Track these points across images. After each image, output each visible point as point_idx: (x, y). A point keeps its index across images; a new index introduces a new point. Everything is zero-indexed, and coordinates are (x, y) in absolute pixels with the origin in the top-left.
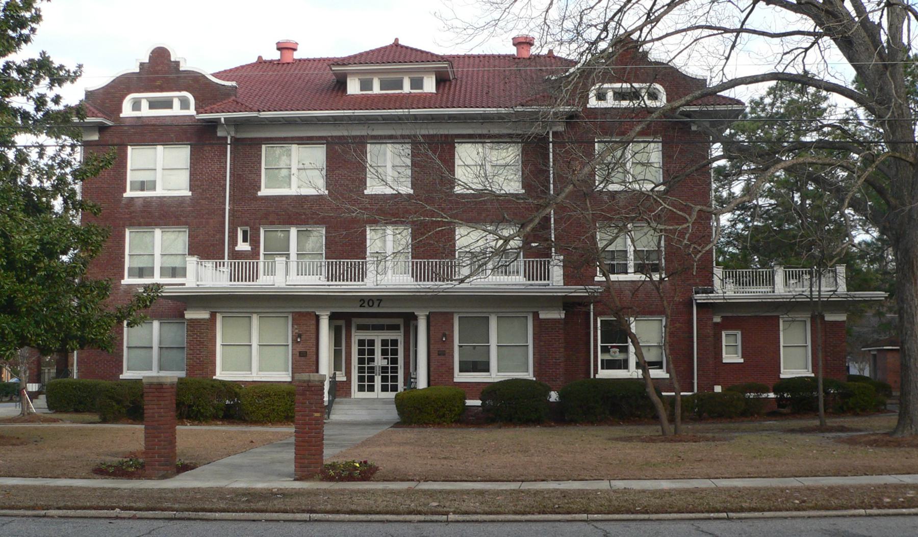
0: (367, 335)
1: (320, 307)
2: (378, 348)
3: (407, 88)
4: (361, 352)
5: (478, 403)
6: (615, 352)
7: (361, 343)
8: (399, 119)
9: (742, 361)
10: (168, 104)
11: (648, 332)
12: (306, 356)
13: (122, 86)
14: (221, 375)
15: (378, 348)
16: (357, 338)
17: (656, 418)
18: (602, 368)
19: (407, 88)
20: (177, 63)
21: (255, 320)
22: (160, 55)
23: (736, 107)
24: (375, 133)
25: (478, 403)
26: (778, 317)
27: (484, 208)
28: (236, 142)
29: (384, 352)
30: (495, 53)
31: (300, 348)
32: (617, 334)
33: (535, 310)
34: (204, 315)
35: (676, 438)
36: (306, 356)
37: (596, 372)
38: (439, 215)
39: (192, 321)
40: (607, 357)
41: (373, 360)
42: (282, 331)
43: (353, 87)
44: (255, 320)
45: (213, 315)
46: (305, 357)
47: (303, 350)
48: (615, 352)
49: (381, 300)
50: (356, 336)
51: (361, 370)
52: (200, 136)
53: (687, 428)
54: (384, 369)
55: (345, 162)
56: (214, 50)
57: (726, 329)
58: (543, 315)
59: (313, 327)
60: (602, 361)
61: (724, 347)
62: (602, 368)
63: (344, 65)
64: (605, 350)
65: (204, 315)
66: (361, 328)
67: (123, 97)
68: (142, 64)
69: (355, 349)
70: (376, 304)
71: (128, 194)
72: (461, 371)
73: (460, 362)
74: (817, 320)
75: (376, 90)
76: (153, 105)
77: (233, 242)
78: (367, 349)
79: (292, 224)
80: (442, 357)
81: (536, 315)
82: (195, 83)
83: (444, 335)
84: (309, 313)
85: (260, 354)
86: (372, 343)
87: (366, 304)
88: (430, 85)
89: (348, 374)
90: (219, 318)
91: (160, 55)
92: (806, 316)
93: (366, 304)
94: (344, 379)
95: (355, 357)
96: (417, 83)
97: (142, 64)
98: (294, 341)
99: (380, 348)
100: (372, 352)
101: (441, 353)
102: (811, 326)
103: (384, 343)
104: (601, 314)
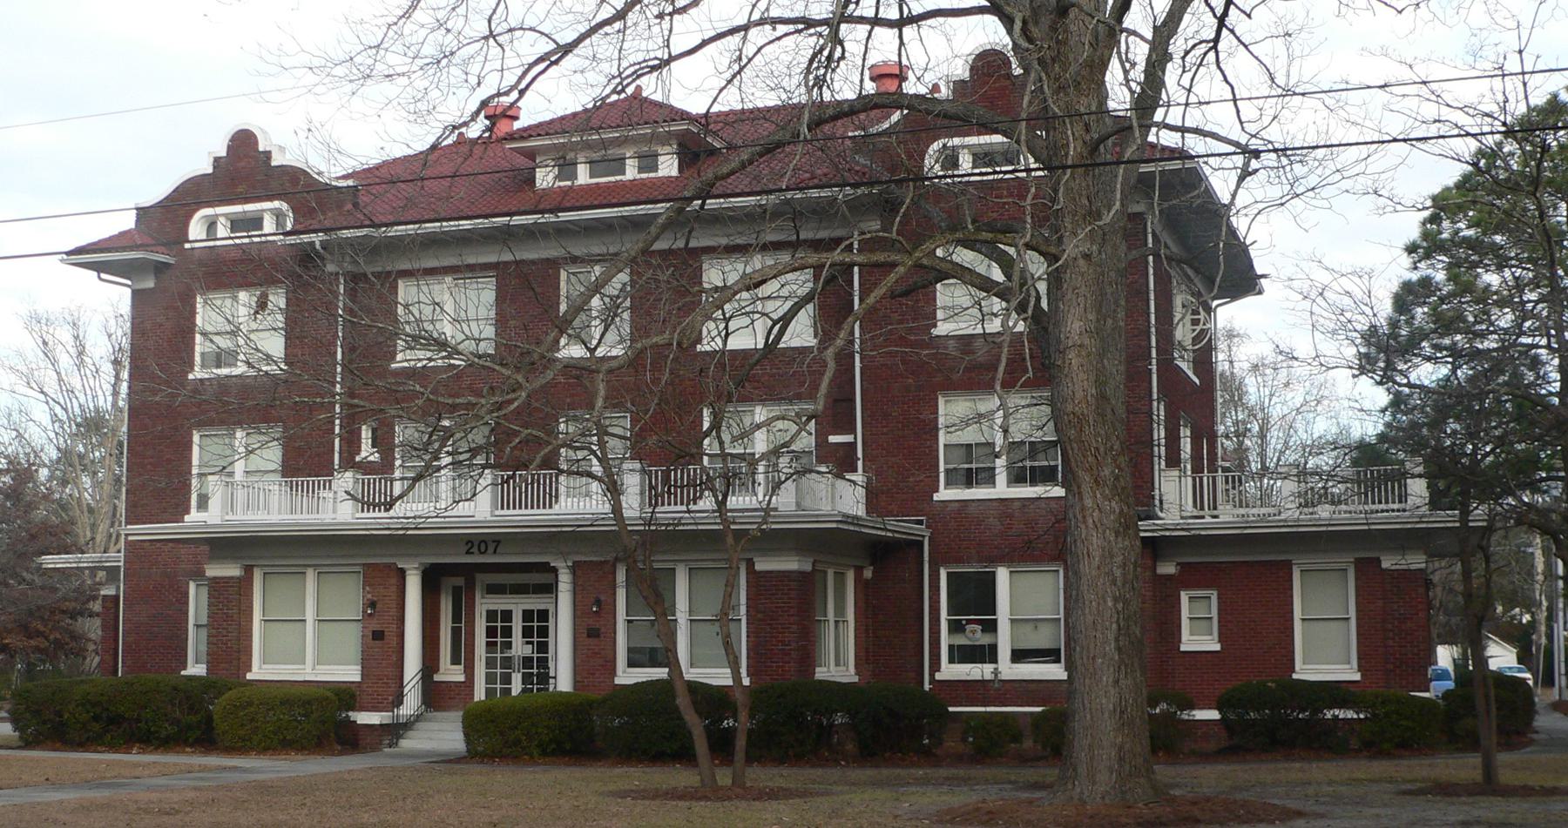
0: (499, 603)
1: (402, 555)
2: (517, 626)
3: (631, 172)
4: (491, 632)
5: (1214, 715)
6: (974, 632)
7: (491, 616)
8: (606, 226)
9: (1217, 647)
10: (236, 224)
11: (1022, 598)
12: (598, 636)
13: (189, 196)
14: (259, 671)
15: (517, 626)
16: (485, 608)
17: (685, 755)
18: (951, 661)
19: (631, 172)
20: (268, 155)
21: (311, 575)
22: (243, 141)
23: (1176, 165)
24: (471, 260)
25: (1214, 715)
26: (1288, 566)
27: (765, 374)
28: (355, 279)
29: (527, 632)
30: (568, 112)
31: (375, 625)
32: (975, 599)
33: (749, 556)
34: (232, 571)
35: (742, 792)
36: (598, 636)
37: (935, 666)
38: (510, 402)
39: (215, 580)
40: (960, 640)
41: (509, 645)
42: (349, 597)
43: (545, 178)
44: (311, 575)
45: (249, 570)
46: (381, 641)
47: (377, 628)
48: (974, 632)
49: (498, 542)
50: (484, 604)
51: (490, 663)
52: (292, 273)
53: (762, 776)
54: (527, 662)
55: (528, 300)
56: (350, 131)
57: (1187, 587)
58: (761, 566)
59: (393, 591)
60: (951, 647)
61: (1185, 623)
62: (951, 661)
63: (522, 138)
64: (956, 627)
65: (232, 571)
66: (493, 590)
67: (189, 216)
68: (217, 160)
69: (481, 627)
70: (491, 550)
71: (198, 373)
72: (630, 665)
73: (630, 650)
74: (1367, 569)
75: (583, 176)
76: (255, 222)
77: (352, 443)
78: (499, 629)
79: (240, 424)
80: (592, 641)
81: (750, 564)
82: (297, 187)
83: (598, 602)
84: (389, 566)
85: (319, 637)
86: (507, 616)
87: (475, 549)
88: (668, 166)
89: (469, 671)
90: (257, 576)
91: (243, 141)
92: (1346, 560)
93: (475, 549)
94: (462, 678)
95: (481, 639)
96: (648, 161)
97: (217, 160)
98: (367, 617)
99: (520, 624)
100: (507, 632)
101: (593, 633)
102: (1357, 579)
103: (528, 615)
104: (946, 562)
